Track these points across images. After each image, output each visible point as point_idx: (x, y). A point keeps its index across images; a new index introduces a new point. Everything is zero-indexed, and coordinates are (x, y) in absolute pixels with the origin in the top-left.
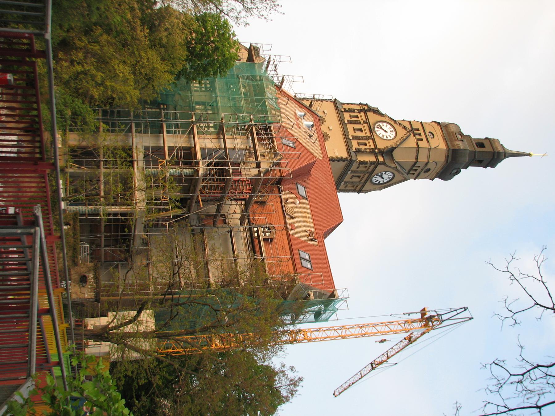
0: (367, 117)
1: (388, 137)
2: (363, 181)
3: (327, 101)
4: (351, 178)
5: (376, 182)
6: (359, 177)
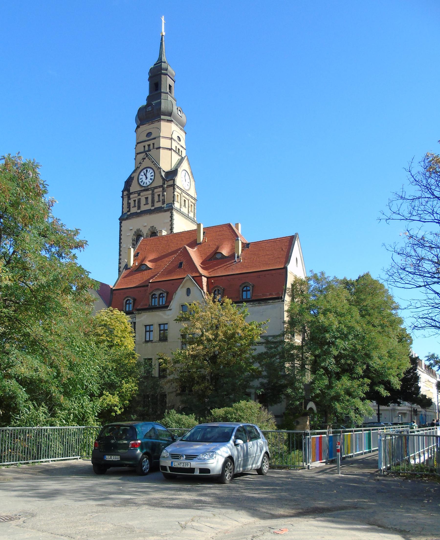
0: (135, 193)
3: (121, 227)
4: (186, 207)
6: (185, 201)
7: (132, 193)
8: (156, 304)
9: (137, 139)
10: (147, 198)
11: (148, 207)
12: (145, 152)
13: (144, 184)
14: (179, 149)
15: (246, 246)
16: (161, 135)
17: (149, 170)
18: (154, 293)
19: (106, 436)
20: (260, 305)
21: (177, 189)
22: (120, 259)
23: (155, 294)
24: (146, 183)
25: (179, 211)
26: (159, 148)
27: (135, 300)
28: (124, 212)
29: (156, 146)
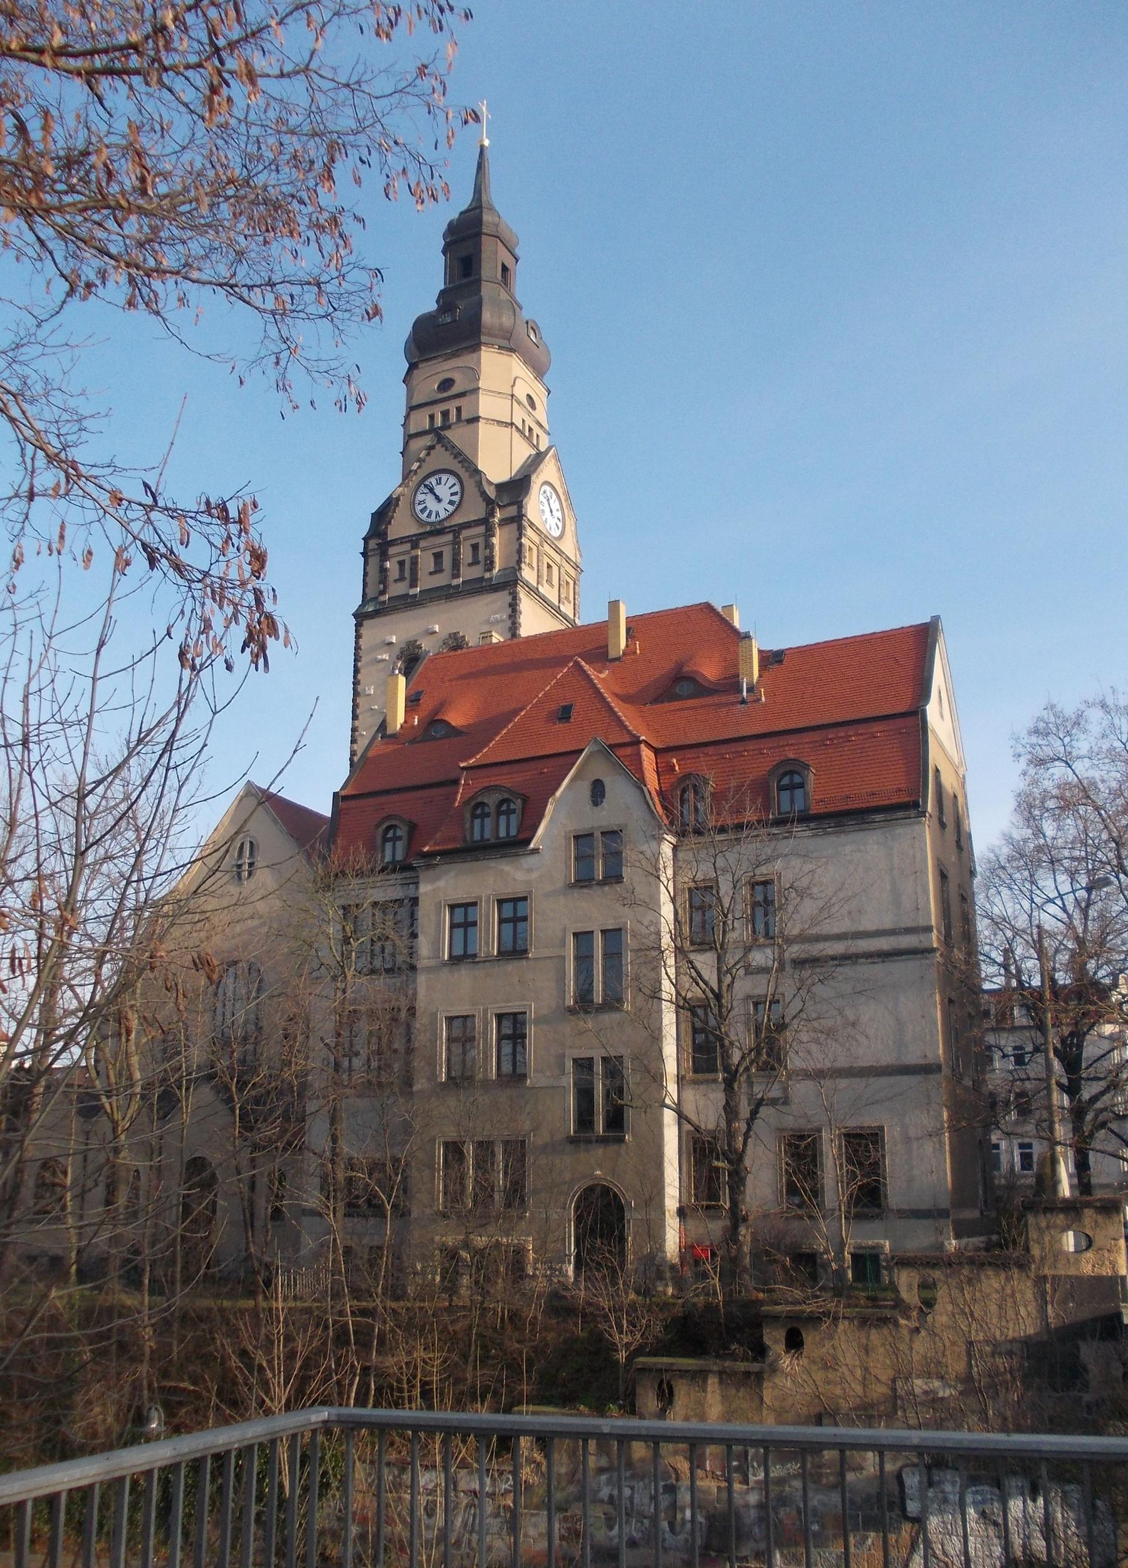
0: (402, 540)
2: (557, 558)
3: (358, 637)
4: (552, 586)
6: (549, 566)
7: (393, 543)
8: (487, 836)
9: (410, 395)
10: (438, 556)
11: (441, 580)
12: (433, 430)
13: (429, 516)
14: (530, 429)
15: (771, 659)
16: (481, 384)
17: (444, 477)
18: (479, 800)
19: (1030, 1187)
20: (844, 832)
21: (529, 529)
22: (354, 730)
23: (482, 804)
24: (437, 514)
25: (534, 591)
26: (476, 419)
27: (413, 827)
28: (369, 597)
29: (464, 416)
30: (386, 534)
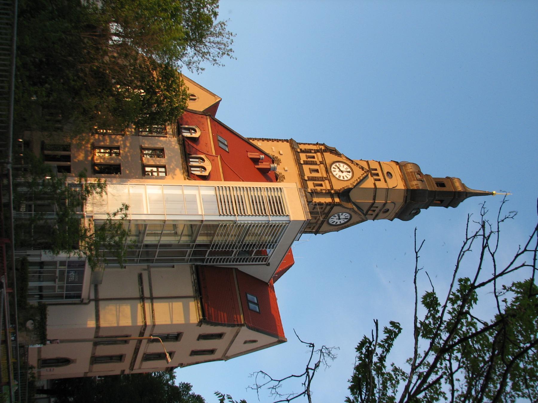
0: (323, 157)
1: (345, 177)
3: (283, 141)
5: (333, 222)
17: (351, 174)
24: (335, 171)
30: (326, 152)
